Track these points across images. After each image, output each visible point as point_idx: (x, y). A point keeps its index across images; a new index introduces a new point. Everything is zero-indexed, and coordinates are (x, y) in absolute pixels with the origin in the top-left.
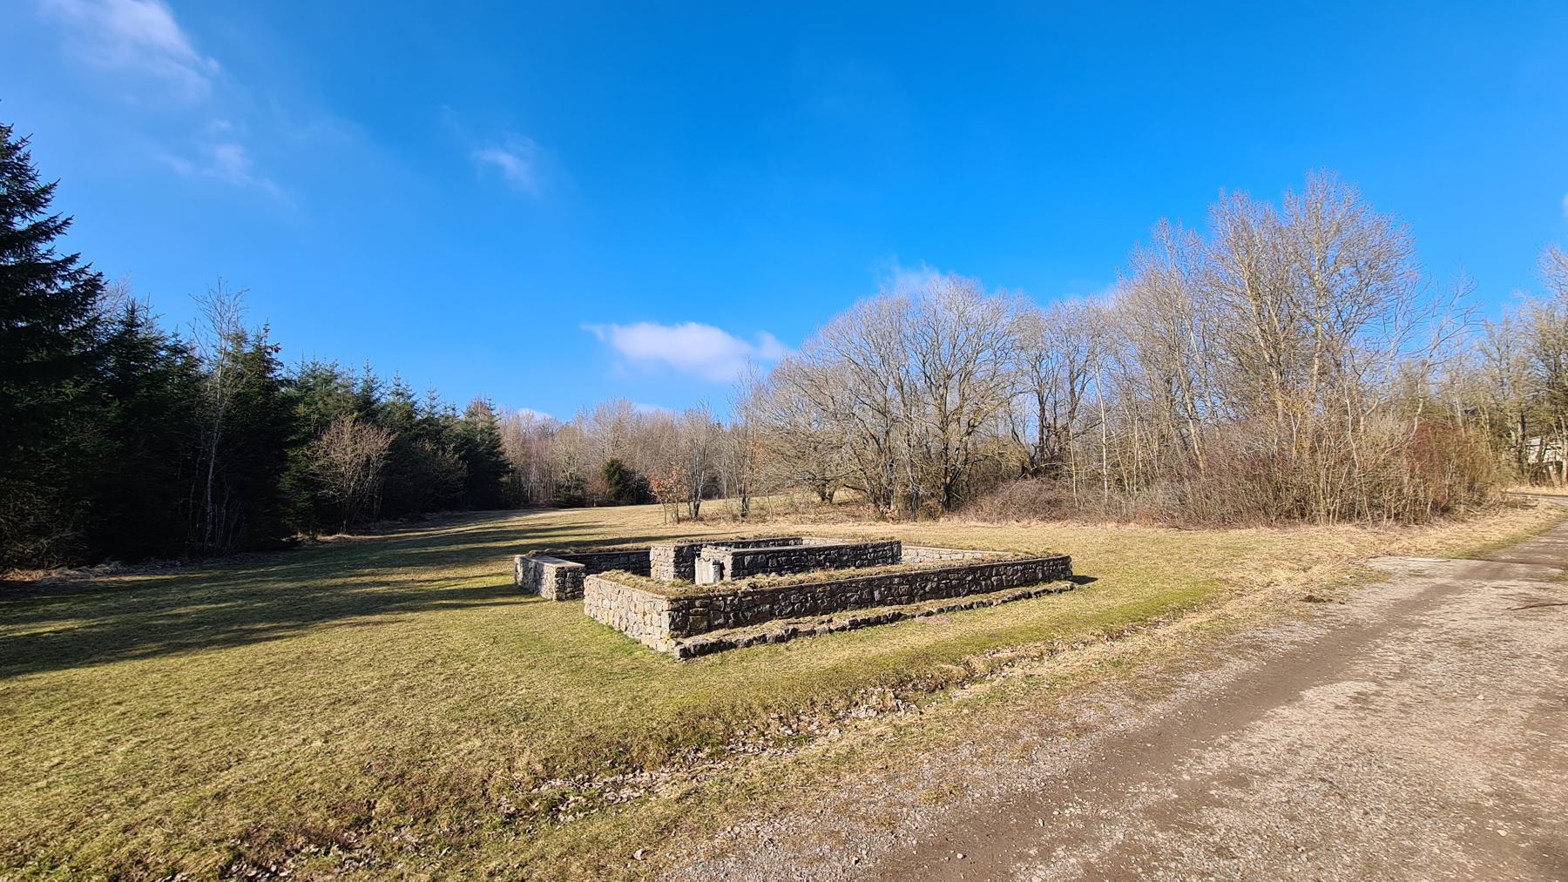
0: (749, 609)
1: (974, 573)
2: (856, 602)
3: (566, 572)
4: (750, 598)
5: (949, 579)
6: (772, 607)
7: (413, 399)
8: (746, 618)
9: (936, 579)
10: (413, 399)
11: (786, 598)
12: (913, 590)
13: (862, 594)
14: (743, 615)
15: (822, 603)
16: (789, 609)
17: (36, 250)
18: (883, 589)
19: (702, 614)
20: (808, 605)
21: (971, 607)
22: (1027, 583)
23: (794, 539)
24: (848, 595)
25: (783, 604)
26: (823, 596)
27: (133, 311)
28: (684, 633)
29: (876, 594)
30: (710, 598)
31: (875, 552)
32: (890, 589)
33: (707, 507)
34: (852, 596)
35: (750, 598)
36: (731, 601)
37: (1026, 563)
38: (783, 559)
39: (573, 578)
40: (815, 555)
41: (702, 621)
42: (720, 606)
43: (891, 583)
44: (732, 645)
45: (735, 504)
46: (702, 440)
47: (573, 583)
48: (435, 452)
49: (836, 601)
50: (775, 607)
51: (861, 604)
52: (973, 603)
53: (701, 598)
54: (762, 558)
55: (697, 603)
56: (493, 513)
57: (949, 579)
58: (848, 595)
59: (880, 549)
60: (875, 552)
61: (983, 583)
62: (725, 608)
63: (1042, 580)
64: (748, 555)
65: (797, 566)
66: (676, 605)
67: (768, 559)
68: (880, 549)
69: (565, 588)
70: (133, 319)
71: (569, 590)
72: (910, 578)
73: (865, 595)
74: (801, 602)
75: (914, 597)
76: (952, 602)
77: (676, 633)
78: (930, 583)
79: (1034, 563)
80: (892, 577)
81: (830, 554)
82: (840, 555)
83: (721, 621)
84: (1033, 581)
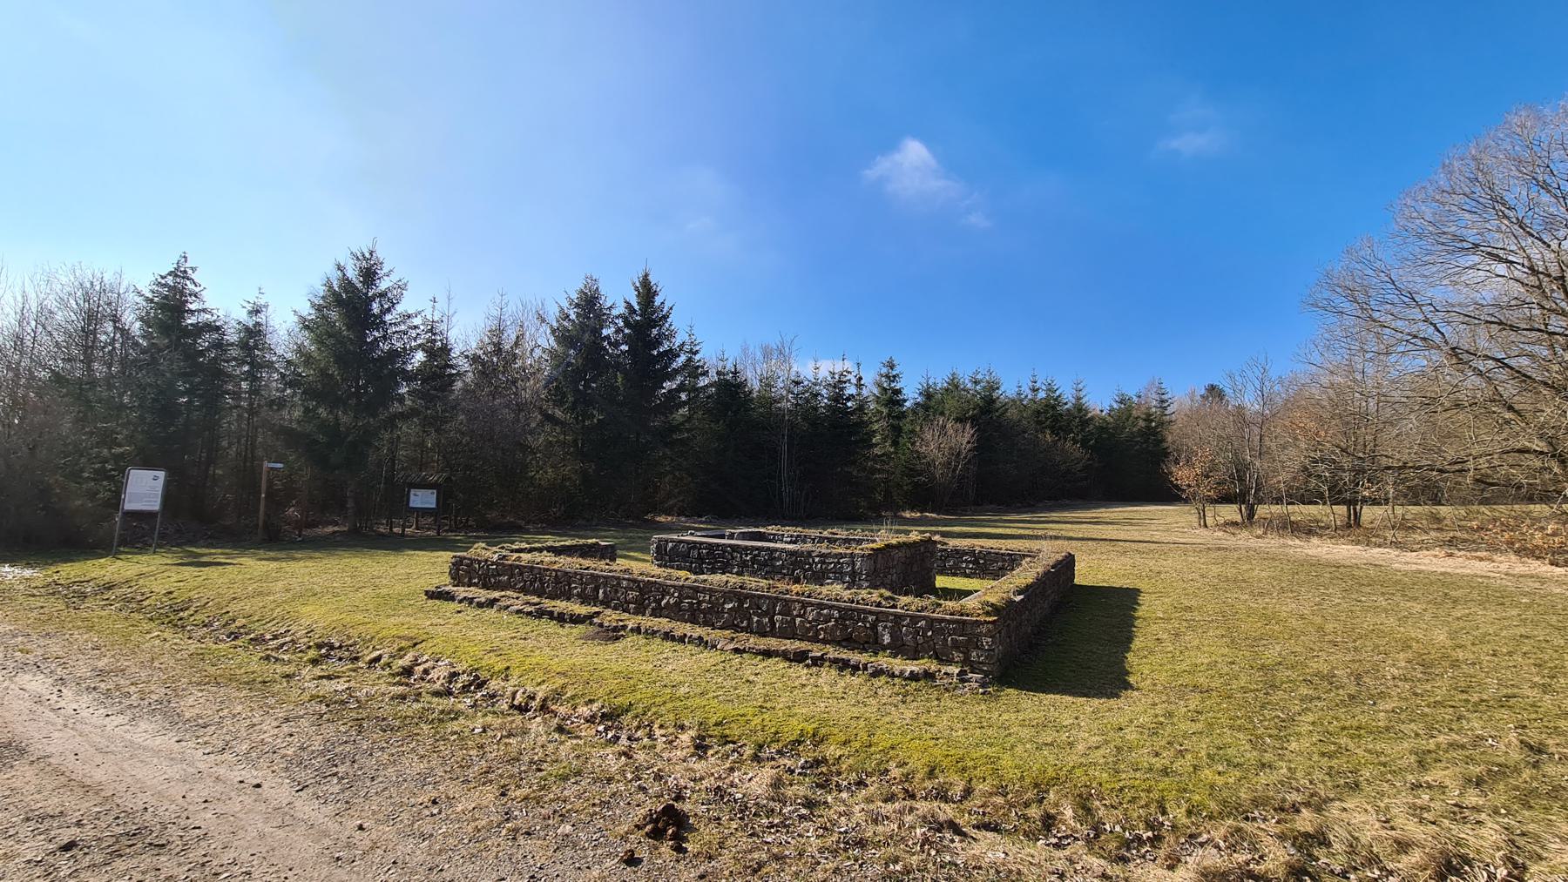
0: (494, 576)
2: (579, 595)
4: (494, 567)
5: (697, 599)
6: (509, 579)
7: (1058, 393)
10: (1058, 393)
11: (521, 574)
15: (548, 587)
18: (609, 589)
22: (848, 642)
26: (549, 580)
31: (823, 563)
34: (576, 588)
35: (494, 567)
40: (741, 554)
43: (619, 584)
46: (1331, 438)
48: (1055, 442)
52: (685, 635)
56: (1136, 503)
57: (697, 599)
60: (823, 563)
65: (719, 562)
73: (588, 590)
74: (530, 581)
75: (645, 609)
76: (773, 643)
81: (759, 555)
82: (773, 559)
83: (476, 580)
84: (873, 645)
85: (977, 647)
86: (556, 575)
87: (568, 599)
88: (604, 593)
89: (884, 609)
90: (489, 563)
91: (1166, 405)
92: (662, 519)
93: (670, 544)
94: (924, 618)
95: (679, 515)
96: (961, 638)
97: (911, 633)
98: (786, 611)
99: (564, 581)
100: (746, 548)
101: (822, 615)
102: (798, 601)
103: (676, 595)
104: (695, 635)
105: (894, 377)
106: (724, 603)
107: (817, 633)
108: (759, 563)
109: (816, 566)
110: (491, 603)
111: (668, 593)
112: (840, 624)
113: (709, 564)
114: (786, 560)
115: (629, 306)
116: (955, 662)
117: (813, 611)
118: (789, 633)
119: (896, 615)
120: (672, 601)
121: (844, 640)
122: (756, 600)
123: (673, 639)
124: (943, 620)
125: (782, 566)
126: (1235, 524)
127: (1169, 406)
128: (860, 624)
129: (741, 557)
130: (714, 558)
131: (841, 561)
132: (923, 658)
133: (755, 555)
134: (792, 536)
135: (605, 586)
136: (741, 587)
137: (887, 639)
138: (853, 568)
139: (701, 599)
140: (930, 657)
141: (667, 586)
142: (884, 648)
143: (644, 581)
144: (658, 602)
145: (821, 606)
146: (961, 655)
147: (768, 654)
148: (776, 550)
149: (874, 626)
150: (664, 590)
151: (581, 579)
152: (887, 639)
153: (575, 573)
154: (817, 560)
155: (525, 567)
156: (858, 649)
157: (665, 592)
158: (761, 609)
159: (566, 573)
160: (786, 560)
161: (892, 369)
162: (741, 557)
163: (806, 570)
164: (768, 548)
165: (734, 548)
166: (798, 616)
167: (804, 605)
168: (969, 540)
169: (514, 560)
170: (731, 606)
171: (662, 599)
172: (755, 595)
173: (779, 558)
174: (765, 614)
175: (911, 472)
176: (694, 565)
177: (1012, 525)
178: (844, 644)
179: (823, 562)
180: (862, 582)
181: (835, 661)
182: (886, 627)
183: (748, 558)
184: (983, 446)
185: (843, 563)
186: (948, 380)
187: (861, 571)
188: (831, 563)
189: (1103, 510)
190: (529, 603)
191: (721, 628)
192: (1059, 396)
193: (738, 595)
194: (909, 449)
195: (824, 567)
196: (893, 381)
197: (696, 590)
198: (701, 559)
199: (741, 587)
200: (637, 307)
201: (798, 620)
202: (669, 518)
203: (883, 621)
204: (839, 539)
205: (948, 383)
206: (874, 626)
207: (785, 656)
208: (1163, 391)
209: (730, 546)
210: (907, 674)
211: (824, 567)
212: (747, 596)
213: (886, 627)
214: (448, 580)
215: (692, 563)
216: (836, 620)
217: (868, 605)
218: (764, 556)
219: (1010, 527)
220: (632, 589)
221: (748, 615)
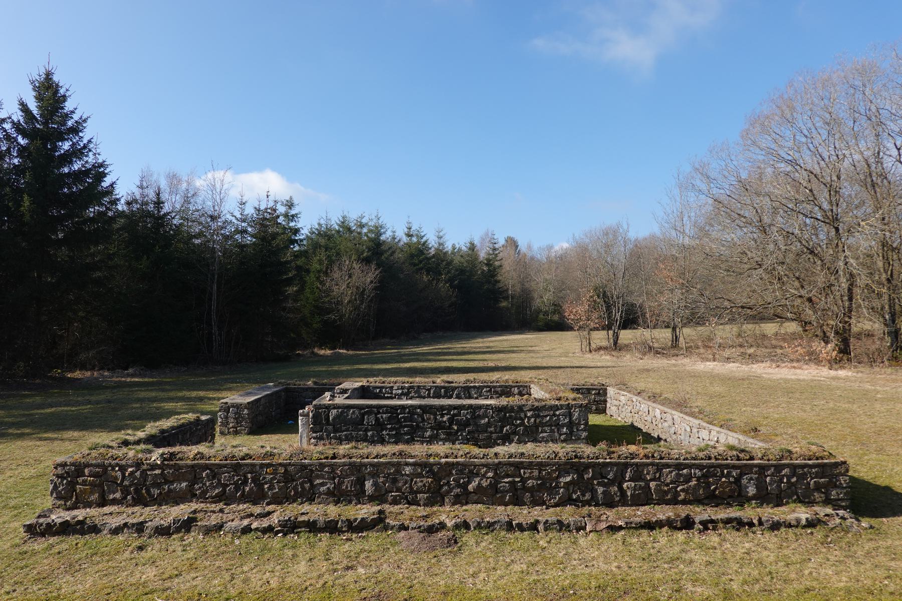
1: (243, 495)
2: (329, 493)
3: (229, 408)
4: (158, 472)
7: (425, 239)
8: (151, 496)
9: (490, 474)
10: (425, 239)
12: (441, 487)
13: (341, 483)
14: (148, 491)
16: (217, 491)
17: (19, 162)
18: (382, 480)
19: (92, 484)
20: (247, 489)
21: (534, 527)
22: (713, 499)
23: (519, 387)
24: (318, 481)
25: (208, 484)
27: (158, 194)
28: (68, 503)
29: (368, 485)
30: (104, 467)
32: (395, 481)
33: (626, 336)
34: (323, 484)
35: (158, 472)
36: (132, 473)
37: (712, 466)
38: (384, 416)
39: (236, 414)
40: (435, 415)
41: (92, 493)
42: (116, 478)
43: (398, 472)
44: (95, 529)
45: (665, 335)
47: (235, 419)
48: (430, 282)
49: (295, 488)
50: (196, 486)
51: (338, 496)
52: (537, 522)
53: (92, 465)
54: (354, 412)
55: (86, 471)
57: (520, 475)
58: (318, 481)
59: (546, 413)
61: (600, 490)
62: (122, 481)
63: (754, 497)
64: (334, 408)
65: (406, 426)
66: (60, 471)
67: (363, 415)
68: (546, 413)
69: (228, 423)
70: (158, 198)
71: (231, 425)
72: (435, 469)
73: (347, 484)
74: (235, 483)
77: (59, 503)
78: (477, 480)
79: (734, 467)
80: (398, 464)
83: (118, 495)
84: (739, 498)
85: (836, 486)
86: (286, 470)
87: (311, 500)
88: (375, 484)
89: (745, 462)
90: (145, 467)
91: (497, 252)
92: (77, 374)
93: (334, 412)
94: (787, 466)
95: (102, 368)
96: (823, 480)
97: (775, 482)
98: (637, 477)
99: (300, 478)
100: (442, 408)
101: (681, 475)
102: (652, 464)
103: (490, 474)
104: (554, 519)
105: (293, 216)
106: (558, 477)
107: (677, 494)
108: (459, 423)
109: (529, 420)
110: (187, 525)
111: (477, 475)
112: (703, 483)
113: (391, 430)
114: (492, 417)
115: (24, 108)
116: (816, 503)
117: (671, 472)
118: (643, 499)
119: (759, 466)
120: (485, 483)
121: (707, 498)
122: (600, 469)
123: (521, 528)
124: (806, 466)
125: (489, 424)
126: (605, 348)
127: (499, 253)
128: (724, 479)
129: (436, 419)
130: (399, 421)
131: (557, 413)
132: (787, 503)
133: (454, 415)
134: (402, 388)
135: (374, 475)
136: (576, 457)
137: (752, 491)
138: (570, 419)
139: (527, 475)
140: (794, 502)
141: (475, 466)
142: (749, 500)
143: (439, 464)
144: (465, 486)
145: (679, 467)
146: (822, 495)
147: (650, 526)
148: (480, 407)
149: (738, 480)
150: (471, 472)
151: (333, 471)
152: (752, 491)
153: (321, 464)
154: (529, 414)
155: (220, 466)
156: (722, 504)
157: (472, 475)
158: (606, 478)
159: (304, 467)
160: (492, 417)
161: (290, 208)
162: (436, 419)
163: (517, 426)
164: (470, 406)
165: (425, 409)
166: (651, 480)
167: (659, 468)
168: (473, 374)
169: (194, 459)
170: (568, 479)
171: (469, 482)
172: (599, 464)
173: (483, 417)
174: (612, 482)
175: (320, 310)
176: (370, 434)
177: (450, 357)
178: (706, 501)
179: (537, 416)
180: (580, 433)
181: (728, 521)
182: (751, 479)
183: (445, 419)
184: (382, 285)
185: (559, 415)
186: (338, 222)
187: (580, 421)
188: (546, 416)
189: (480, 340)
190: (252, 515)
191: (556, 505)
192: (426, 241)
193: (575, 465)
194: (318, 288)
195: (538, 421)
196: (292, 221)
197: (518, 466)
198: (379, 426)
199: (576, 457)
200: (35, 111)
201: (653, 485)
202: (88, 374)
203: (748, 474)
204: (458, 387)
205: (339, 225)
206: (738, 480)
207: (670, 525)
208: (496, 241)
209: (420, 407)
210: (804, 522)
211: (538, 421)
212: (587, 466)
213: (751, 479)
214: (49, 502)
215: (366, 430)
216: (698, 479)
217: (727, 459)
218: (465, 415)
219: (461, 360)
220: (420, 475)
221: (590, 487)
